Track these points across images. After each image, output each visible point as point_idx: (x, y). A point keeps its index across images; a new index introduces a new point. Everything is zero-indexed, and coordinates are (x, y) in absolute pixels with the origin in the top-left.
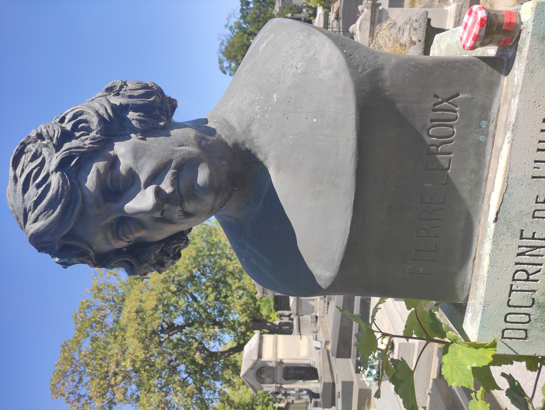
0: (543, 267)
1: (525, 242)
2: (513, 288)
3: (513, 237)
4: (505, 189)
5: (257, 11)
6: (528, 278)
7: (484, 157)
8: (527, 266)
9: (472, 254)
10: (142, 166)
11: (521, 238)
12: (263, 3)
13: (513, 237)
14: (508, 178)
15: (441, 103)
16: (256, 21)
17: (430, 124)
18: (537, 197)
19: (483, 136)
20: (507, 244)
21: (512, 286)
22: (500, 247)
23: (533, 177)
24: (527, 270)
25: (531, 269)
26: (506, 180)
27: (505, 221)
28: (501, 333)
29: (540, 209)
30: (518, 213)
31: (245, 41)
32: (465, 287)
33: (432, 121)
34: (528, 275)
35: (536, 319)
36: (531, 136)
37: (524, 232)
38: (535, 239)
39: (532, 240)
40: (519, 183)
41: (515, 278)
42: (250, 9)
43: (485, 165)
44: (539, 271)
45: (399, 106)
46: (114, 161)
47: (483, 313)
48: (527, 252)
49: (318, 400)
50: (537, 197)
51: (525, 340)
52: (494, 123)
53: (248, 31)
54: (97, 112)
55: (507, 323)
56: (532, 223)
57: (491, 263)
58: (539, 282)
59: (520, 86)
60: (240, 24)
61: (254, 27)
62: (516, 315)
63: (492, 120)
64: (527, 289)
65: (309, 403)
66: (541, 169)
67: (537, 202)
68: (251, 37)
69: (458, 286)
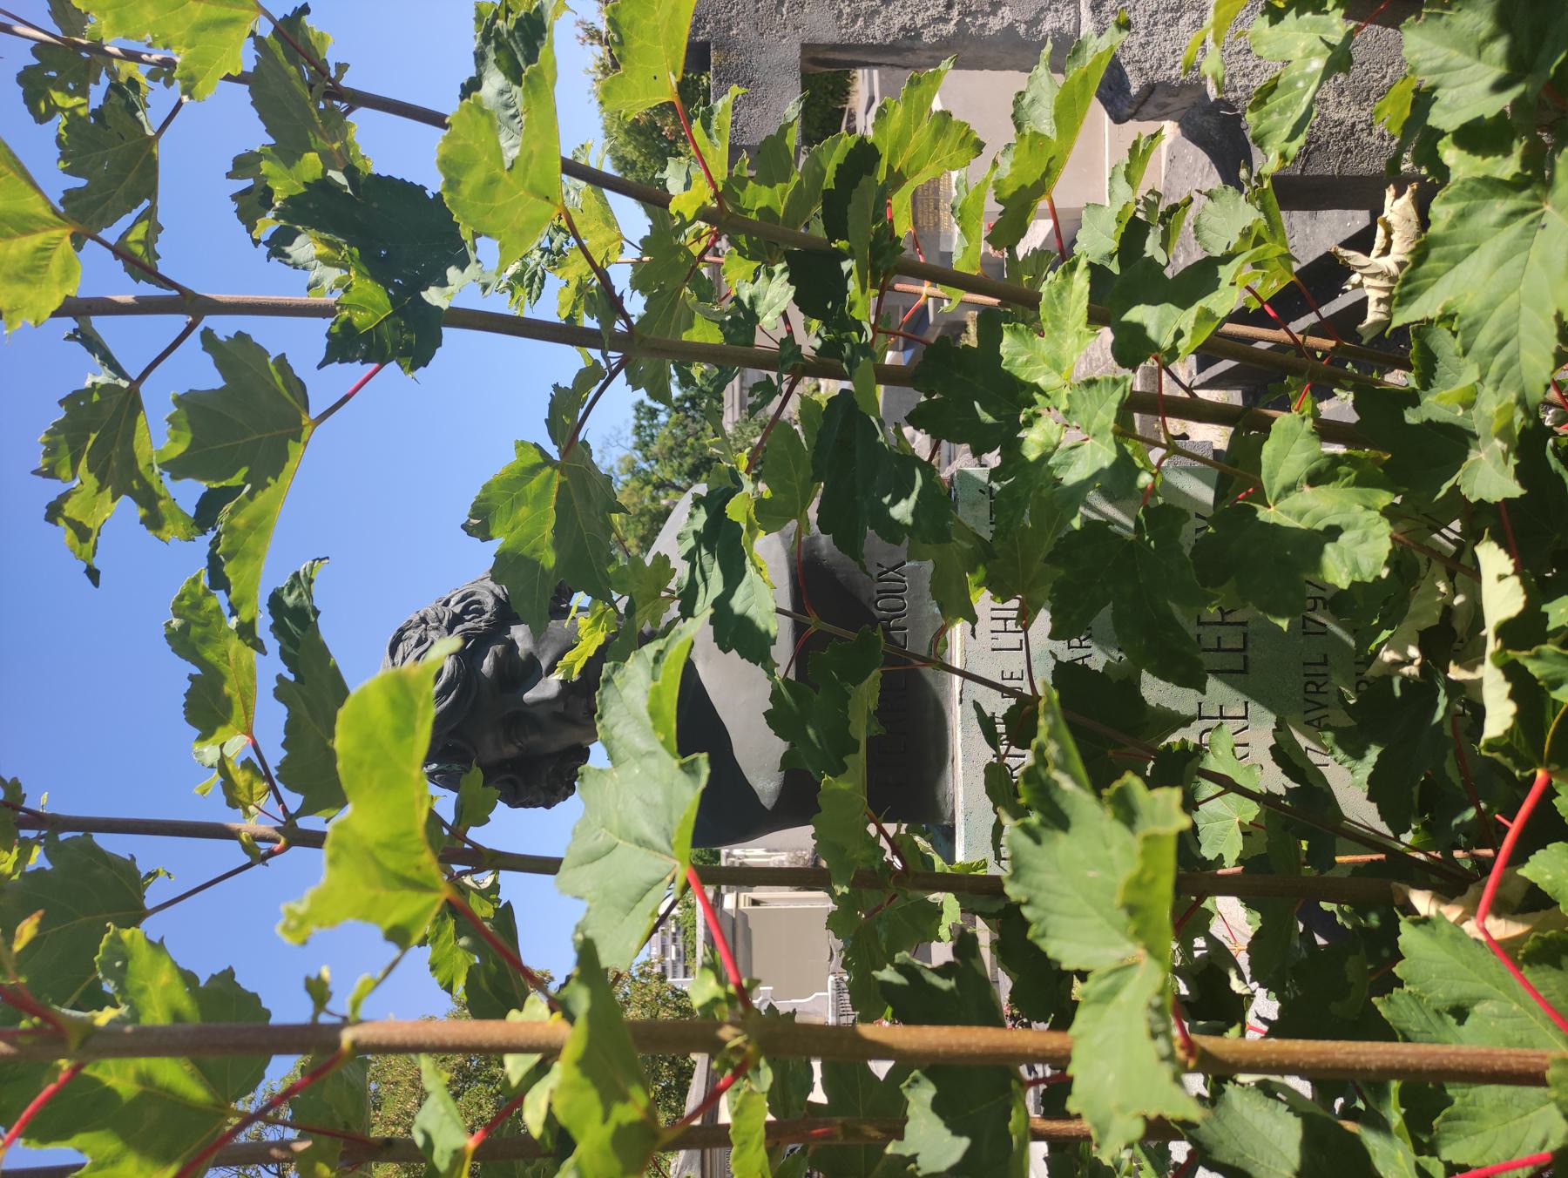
5: (677, 432)
10: (544, 651)
12: (691, 413)
15: (886, 572)
16: (675, 453)
17: (876, 596)
31: (647, 501)
33: (879, 592)
42: (657, 426)
45: (839, 576)
46: (512, 645)
53: (654, 478)
54: (494, 595)
60: (634, 462)
61: (669, 468)
68: (661, 493)
69: (940, 797)
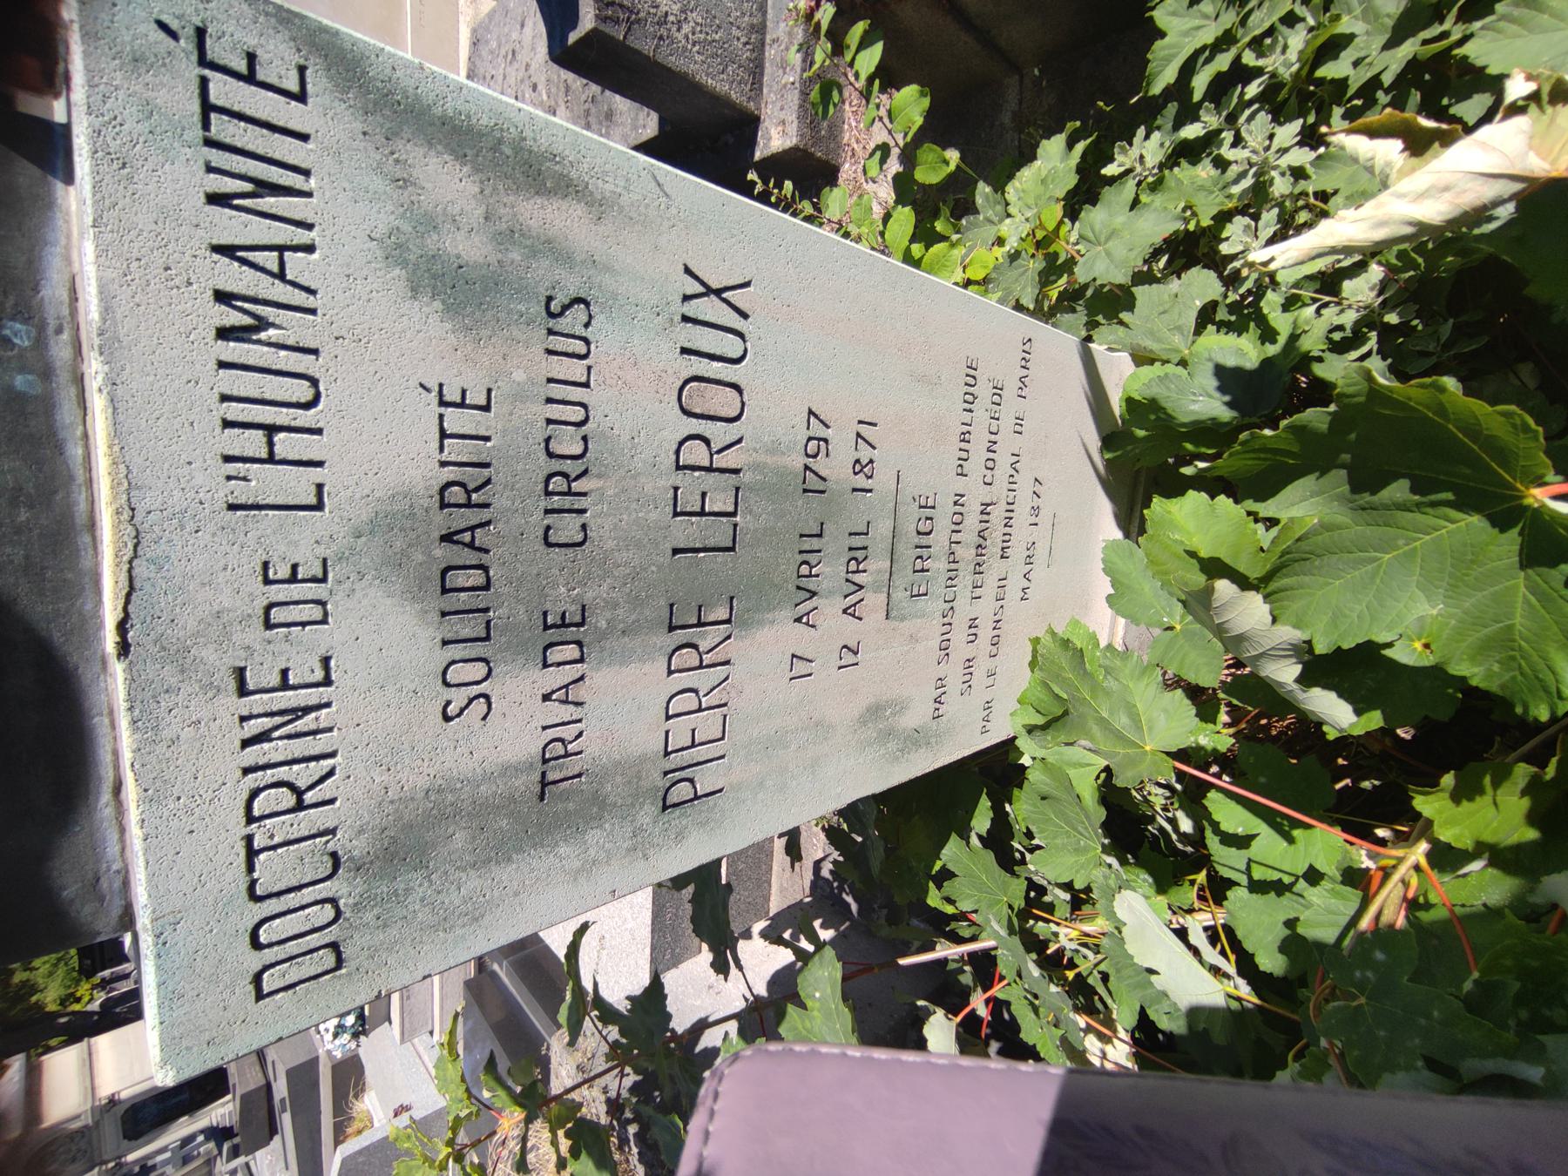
0: (339, 758)
1: (257, 703)
2: (256, 845)
3: (210, 694)
4: (130, 546)
6: (300, 801)
7: (59, 448)
8: (287, 768)
9: (103, 772)
11: (243, 691)
13: (210, 694)
14: (133, 510)
18: (266, 565)
19: (30, 377)
20: (194, 719)
21: (249, 839)
22: (167, 734)
23: (233, 507)
24: (292, 779)
25: (302, 775)
26: (126, 515)
27: (164, 649)
28: (251, 988)
29: (284, 600)
30: (210, 620)
32: (104, 884)
34: (299, 793)
35: (356, 904)
36: (185, 377)
37: (248, 674)
38: (294, 688)
39: (281, 694)
40: (182, 527)
41: (256, 813)
43: (71, 478)
44: (331, 773)
47: (159, 956)
48: (277, 728)
49: (237, 1140)
50: (266, 565)
51: (338, 973)
52: (65, 336)
55: (266, 951)
56: (269, 642)
57: (146, 790)
58: (338, 804)
59: (89, 202)
62: (289, 917)
63: (52, 324)
64: (307, 833)
65: (215, 1158)
66: (253, 483)
67: (546, 627)
